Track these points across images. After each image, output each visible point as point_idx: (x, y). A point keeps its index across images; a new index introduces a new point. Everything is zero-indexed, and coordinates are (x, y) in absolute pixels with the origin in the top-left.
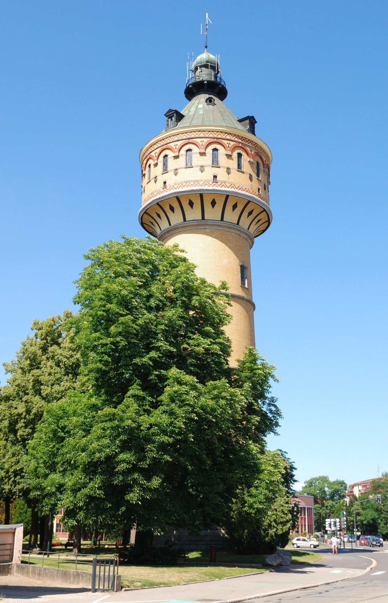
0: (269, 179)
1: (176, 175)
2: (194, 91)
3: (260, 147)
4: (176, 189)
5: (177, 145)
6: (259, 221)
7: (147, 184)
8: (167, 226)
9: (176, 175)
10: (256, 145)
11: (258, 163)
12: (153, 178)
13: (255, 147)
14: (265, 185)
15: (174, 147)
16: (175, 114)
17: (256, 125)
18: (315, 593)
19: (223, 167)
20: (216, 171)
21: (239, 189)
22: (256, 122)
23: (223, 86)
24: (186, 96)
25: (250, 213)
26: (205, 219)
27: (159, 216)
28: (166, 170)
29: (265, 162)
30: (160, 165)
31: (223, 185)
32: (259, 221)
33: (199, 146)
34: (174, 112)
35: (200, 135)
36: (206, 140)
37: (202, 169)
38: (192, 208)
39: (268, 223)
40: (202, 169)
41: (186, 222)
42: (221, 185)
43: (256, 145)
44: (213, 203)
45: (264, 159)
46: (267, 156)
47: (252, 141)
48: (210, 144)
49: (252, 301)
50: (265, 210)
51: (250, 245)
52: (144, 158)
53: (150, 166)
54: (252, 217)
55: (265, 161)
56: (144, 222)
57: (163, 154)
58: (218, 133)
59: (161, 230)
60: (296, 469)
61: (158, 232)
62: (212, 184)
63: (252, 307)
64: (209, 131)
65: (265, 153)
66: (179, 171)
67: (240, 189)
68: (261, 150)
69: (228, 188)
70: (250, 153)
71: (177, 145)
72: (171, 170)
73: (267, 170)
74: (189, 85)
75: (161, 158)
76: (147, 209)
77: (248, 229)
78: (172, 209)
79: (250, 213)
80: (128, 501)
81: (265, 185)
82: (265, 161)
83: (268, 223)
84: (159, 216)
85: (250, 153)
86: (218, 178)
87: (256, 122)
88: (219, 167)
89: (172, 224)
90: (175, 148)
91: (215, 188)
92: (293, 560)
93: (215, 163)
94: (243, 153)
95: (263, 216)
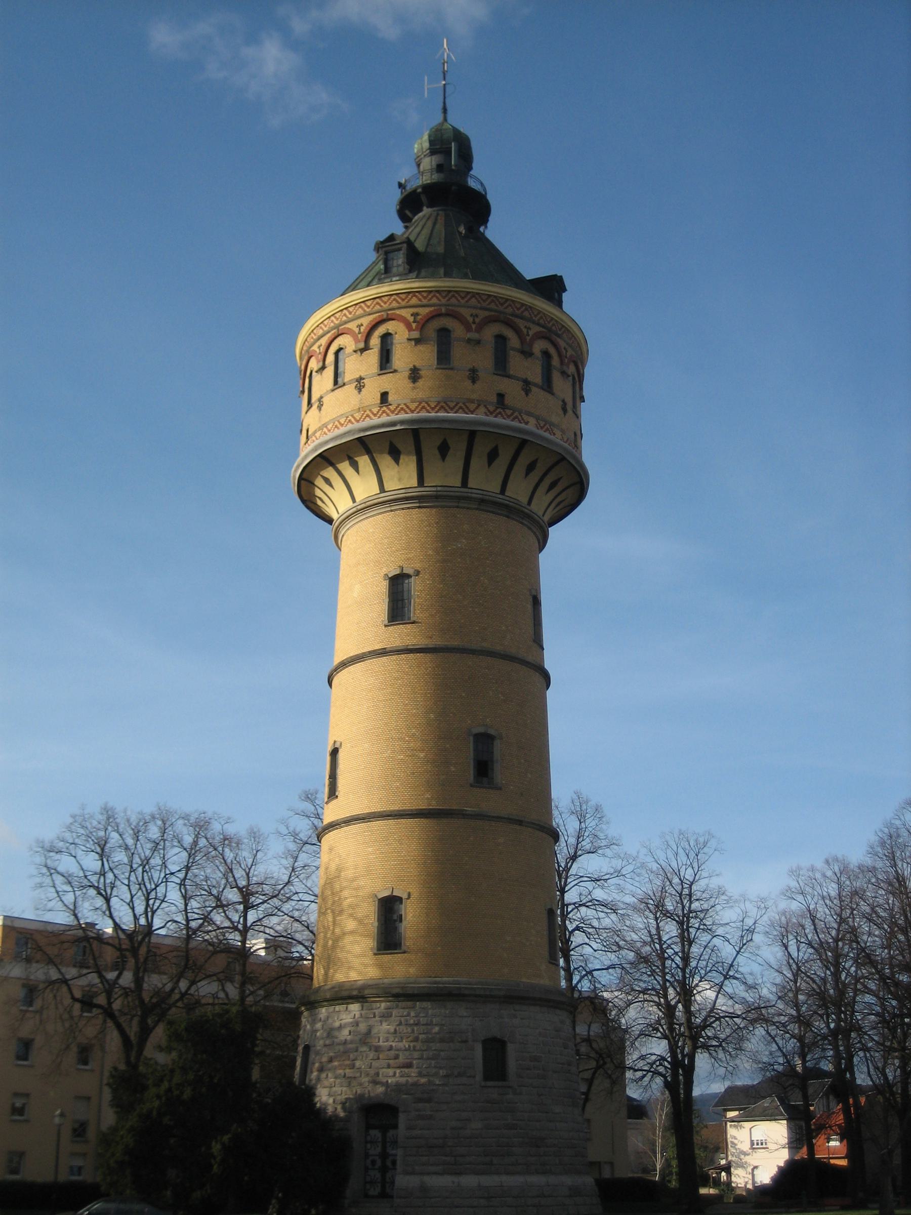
1: (360, 390)
2: (423, 198)
4: (358, 421)
7: (306, 413)
8: (350, 504)
9: (360, 390)
12: (315, 402)
16: (405, 245)
18: (367, 272)
19: (517, 379)
21: (399, 412)
26: (469, 486)
28: (340, 380)
29: (565, 352)
30: (329, 372)
31: (516, 417)
35: (409, 300)
36: (487, 313)
38: (398, 464)
40: (473, 375)
42: (457, 408)
45: (562, 344)
48: (495, 320)
50: (563, 459)
54: (535, 476)
55: (565, 348)
58: (432, 294)
62: (494, 411)
63: (542, 680)
64: (431, 292)
67: (516, 417)
69: (472, 413)
71: (477, 316)
72: (350, 382)
75: (330, 358)
79: (531, 468)
80: (382, 1086)
82: (565, 348)
86: (508, 401)
88: (452, 369)
89: (358, 499)
90: (357, 332)
91: (499, 420)
92: (738, 1195)
93: (501, 365)
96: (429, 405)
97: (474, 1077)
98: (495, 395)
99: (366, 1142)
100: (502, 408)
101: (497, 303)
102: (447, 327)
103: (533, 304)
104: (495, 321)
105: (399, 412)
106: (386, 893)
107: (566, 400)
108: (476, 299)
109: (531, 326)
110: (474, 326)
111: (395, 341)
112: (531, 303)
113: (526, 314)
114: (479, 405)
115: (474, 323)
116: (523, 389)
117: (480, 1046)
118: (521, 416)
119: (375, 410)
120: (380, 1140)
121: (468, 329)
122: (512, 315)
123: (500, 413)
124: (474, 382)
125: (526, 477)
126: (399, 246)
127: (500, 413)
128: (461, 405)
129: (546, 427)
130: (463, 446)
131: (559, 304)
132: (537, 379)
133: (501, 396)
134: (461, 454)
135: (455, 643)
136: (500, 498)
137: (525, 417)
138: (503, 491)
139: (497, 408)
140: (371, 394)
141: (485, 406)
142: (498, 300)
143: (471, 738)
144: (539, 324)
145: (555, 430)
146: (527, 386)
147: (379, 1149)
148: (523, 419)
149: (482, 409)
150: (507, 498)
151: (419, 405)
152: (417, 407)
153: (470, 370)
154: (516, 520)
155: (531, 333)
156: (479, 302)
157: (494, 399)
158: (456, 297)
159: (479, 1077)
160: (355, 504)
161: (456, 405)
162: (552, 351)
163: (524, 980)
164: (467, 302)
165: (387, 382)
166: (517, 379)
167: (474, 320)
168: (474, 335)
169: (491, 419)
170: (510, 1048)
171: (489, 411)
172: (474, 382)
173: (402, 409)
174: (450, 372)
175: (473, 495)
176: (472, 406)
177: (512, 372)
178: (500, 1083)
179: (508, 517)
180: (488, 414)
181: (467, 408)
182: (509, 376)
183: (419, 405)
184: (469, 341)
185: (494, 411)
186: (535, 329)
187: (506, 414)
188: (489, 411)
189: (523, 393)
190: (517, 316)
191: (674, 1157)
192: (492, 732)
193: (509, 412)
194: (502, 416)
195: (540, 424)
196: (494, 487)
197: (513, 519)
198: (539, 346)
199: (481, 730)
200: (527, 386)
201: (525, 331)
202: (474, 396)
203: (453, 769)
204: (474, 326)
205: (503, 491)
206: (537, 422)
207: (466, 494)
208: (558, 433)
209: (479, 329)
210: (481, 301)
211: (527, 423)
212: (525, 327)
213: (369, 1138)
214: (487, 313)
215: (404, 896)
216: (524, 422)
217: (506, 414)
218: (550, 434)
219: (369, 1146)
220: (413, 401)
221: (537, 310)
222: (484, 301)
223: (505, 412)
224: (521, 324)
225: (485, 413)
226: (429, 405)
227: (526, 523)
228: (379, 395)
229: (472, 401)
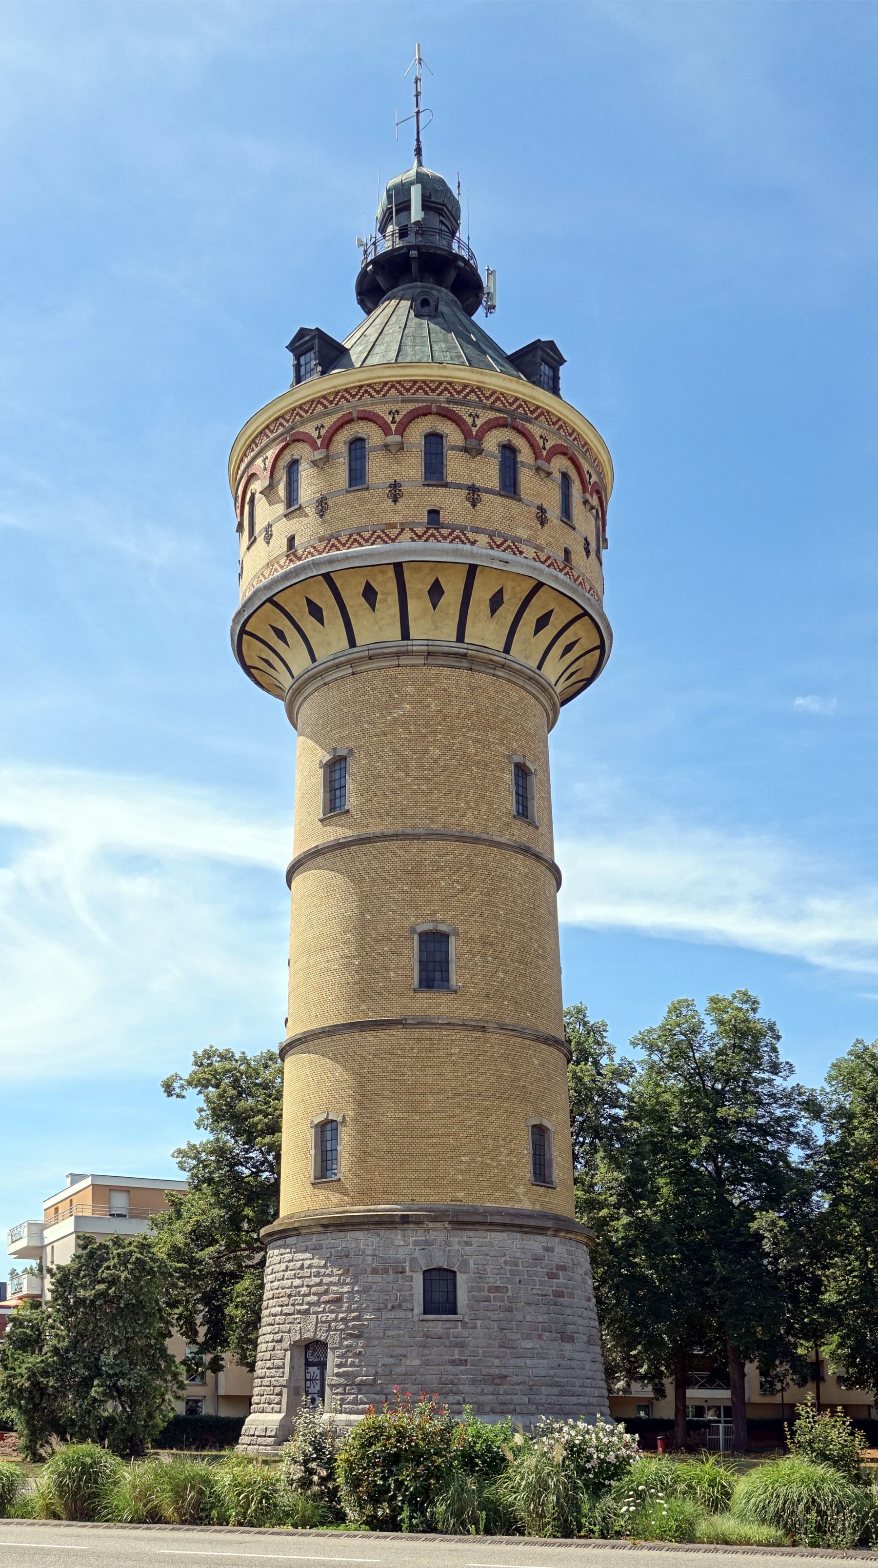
0: (604, 530)
3: (574, 431)
5: (397, 412)
6: (569, 648)
8: (291, 681)
10: (560, 423)
11: (565, 476)
13: (558, 429)
14: (587, 543)
15: (315, 434)
16: (316, 341)
17: (563, 370)
19: (459, 486)
20: (438, 498)
22: (562, 361)
23: (466, 262)
24: (361, 302)
25: (542, 622)
27: (280, 635)
29: (588, 476)
31: (458, 537)
32: (569, 648)
33: (374, 419)
34: (313, 334)
37: (395, 492)
39: (598, 652)
40: (395, 492)
41: (355, 649)
43: (557, 423)
44: (370, 594)
45: (586, 467)
46: (595, 461)
47: (548, 412)
48: (414, 416)
49: (553, 861)
51: (548, 715)
52: (238, 477)
53: (253, 495)
56: (249, 663)
57: (286, 459)
59: (293, 677)
60: (195, 1054)
61: (286, 682)
62: (425, 533)
65: (587, 450)
66: (485, 497)
68: (575, 439)
70: (541, 445)
71: (397, 412)
73: (595, 501)
74: (367, 265)
76: (246, 615)
77: (539, 667)
78: (316, 612)
79: (542, 622)
81: (587, 543)
83: (598, 652)
84: (280, 635)
85: (541, 445)
86: (444, 517)
87: (562, 361)
88: (367, 489)
94: (519, 442)
95: (589, 640)
96: (339, 541)
97: (412, 1310)
98: (426, 514)
99: (306, 1380)
100: (435, 529)
101: (427, 389)
102: (359, 435)
103: (481, 382)
104: (425, 415)
105: (352, 544)
106: (322, 1118)
107: (545, 506)
108: (397, 389)
109: (480, 412)
110: (393, 427)
111: (300, 469)
112: (478, 382)
113: (473, 397)
114: (403, 530)
115: (393, 422)
116: (538, 518)
117: (422, 1276)
118: (465, 535)
119: (419, 531)
120: (318, 1377)
121: (387, 431)
122: (448, 402)
123: (433, 535)
124: (395, 501)
125: (492, 615)
126: (309, 344)
127: (433, 535)
128: (379, 533)
129: (506, 545)
130: (393, 586)
131: (555, 390)
132: (494, 483)
133: (434, 514)
134: (394, 599)
135: (399, 828)
136: (459, 648)
137: (471, 535)
138: (460, 638)
139: (428, 529)
140: (279, 543)
141: (412, 529)
142: (428, 386)
143: (416, 937)
144: (492, 408)
145: (523, 548)
146: (474, 493)
147: (318, 1387)
148: (467, 538)
149: (408, 534)
150: (470, 647)
151: (328, 543)
152: (326, 547)
153: (390, 486)
154: (483, 672)
155: (479, 422)
156: (401, 394)
157: (424, 518)
158: (369, 394)
159: (418, 1308)
160: (538, 671)
161: (349, 538)
162: (519, 442)
163: (488, 1204)
164: (384, 395)
165: (294, 526)
166: (459, 486)
167: (394, 418)
168: (394, 439)
169: (420, 544)
170: (461, 1279)
171: (416, 534)
172: (395, 501)
173: (379, 537)
174: (365, 494)
175: (415, 648)
176: (393, 533)
177: (449, 480)
178: (450, 1317)
179: (471, 669)
180: (416, 538)
181: (387, 535)
182: (446, 485)
183: (328, 543)
184: (386, 447)
185: (425, 533)
186: (486, 416)
187: (442, 536)
188: (416, 534)
189: (468, 505)
190: (456, 403)
191: (865, 1089)
192: (443, 928)
193: (446, 532)
194: (436, 538)
195: (495, 543)
196: (449, 632)
197: (479, 671)
198: (559, 464)
199: (428, 927)
200: (474, 493)
201: (469, 421)
202: (396, 519)
203: (392, 974)
204: (393, 427)
205: (460, 638)
206: (491, 539)
207: (403, 649)
208: (529, 552)
209: (401, 431)
210: (404, 392)
211: (473, 543)
212: (470, 415)
213: (308, 1377)
214: (411, 406)
215: (339, 1119)
216: (469, 542)
217: (442, 536)
218: (515, 554)
219: (308, 1383)
220: (321, 540)
221: (556, 416)
222: (408, 390)
223: (439, 533)
224: (463, 412)
225: (412, 539)
226: (339, 541)
227: (500, 674)
228: (286, 540)
229: (393, 526)
